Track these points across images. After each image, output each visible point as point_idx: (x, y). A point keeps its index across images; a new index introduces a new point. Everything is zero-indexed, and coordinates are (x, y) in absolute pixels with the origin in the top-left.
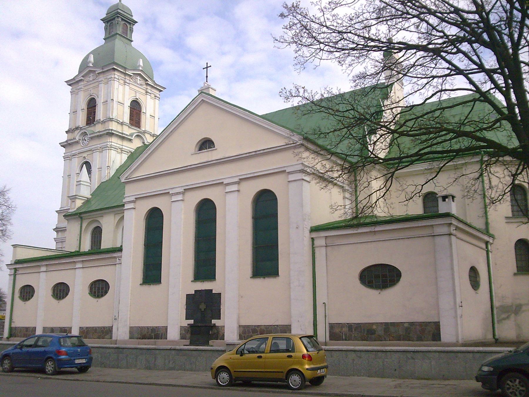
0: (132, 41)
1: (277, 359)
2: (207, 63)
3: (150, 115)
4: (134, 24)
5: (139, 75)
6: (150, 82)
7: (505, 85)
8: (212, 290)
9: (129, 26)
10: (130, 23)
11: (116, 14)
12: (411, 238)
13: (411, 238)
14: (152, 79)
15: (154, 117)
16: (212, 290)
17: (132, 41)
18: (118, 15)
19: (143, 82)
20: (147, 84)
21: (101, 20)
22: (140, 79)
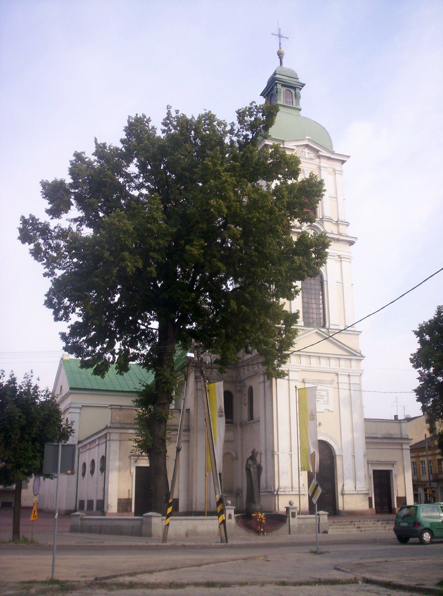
0: (300, 110)
1: (107, 395)
2: (273, 34)
3: (330, 197)
4: (301, 87)
5: (307, 146)
6: (323, 153)
7: (150, 465)
8: (19, 229)
9: (293, 91)
10: (294, 88)
11: (273, 82)
12: (324, 372)
13: (324, 372)
14: (333, 153)
15: (337, 199)
16: (19, 229)
17: (300, 110)
18: (276, 82)
19: (312, 155)
20: (319, 157)
21: (260, 95)
22: (309, 151)
